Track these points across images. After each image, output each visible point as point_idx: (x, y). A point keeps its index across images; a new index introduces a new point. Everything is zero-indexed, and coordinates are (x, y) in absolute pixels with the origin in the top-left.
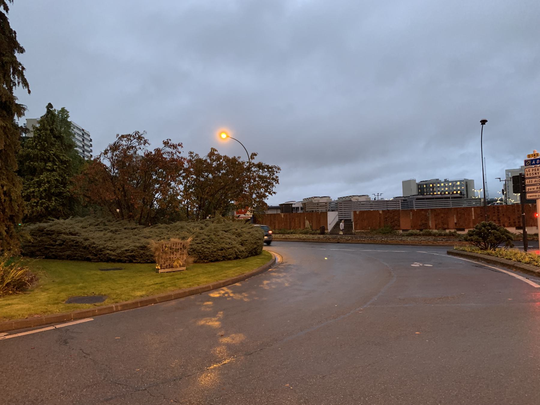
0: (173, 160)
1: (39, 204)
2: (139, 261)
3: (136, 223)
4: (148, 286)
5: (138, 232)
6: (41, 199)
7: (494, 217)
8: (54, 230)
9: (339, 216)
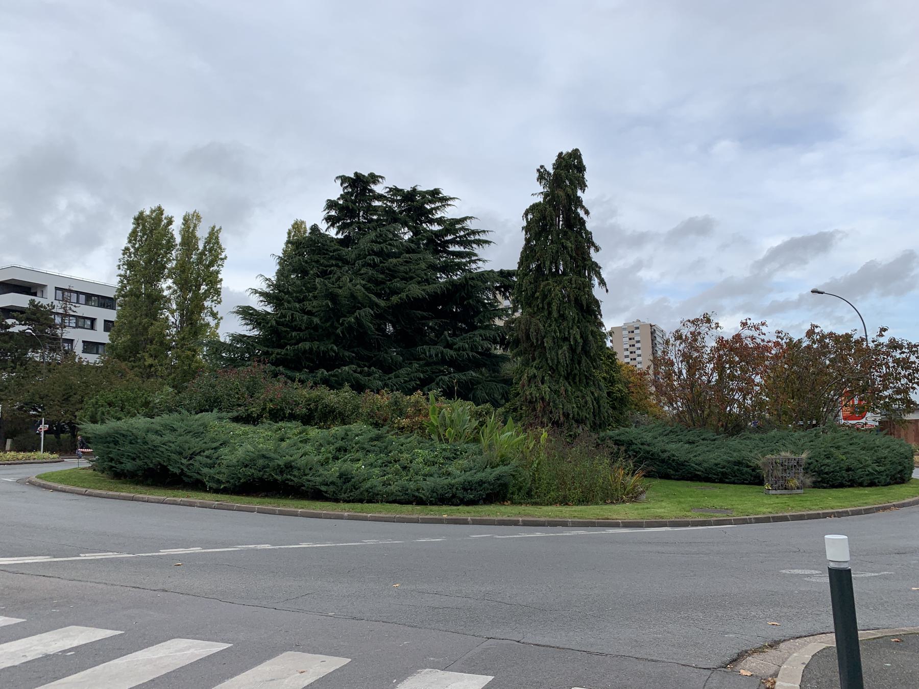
0: (758, 347)
8: (623, 441)
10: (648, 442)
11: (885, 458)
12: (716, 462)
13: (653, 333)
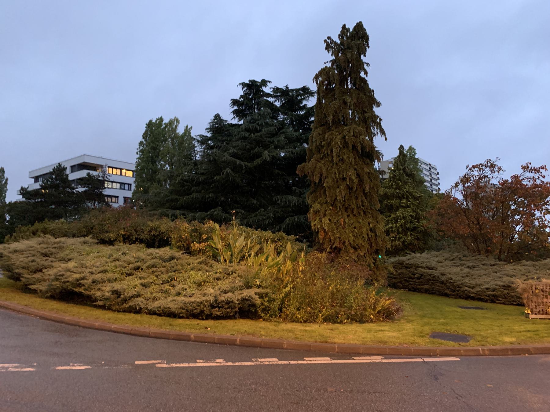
1: (397, 239)
2: (502, 302)
3: (495, 259)
4: (517, 332)
5: (498, 268)
6: (398, 233)
8: (412, 264)
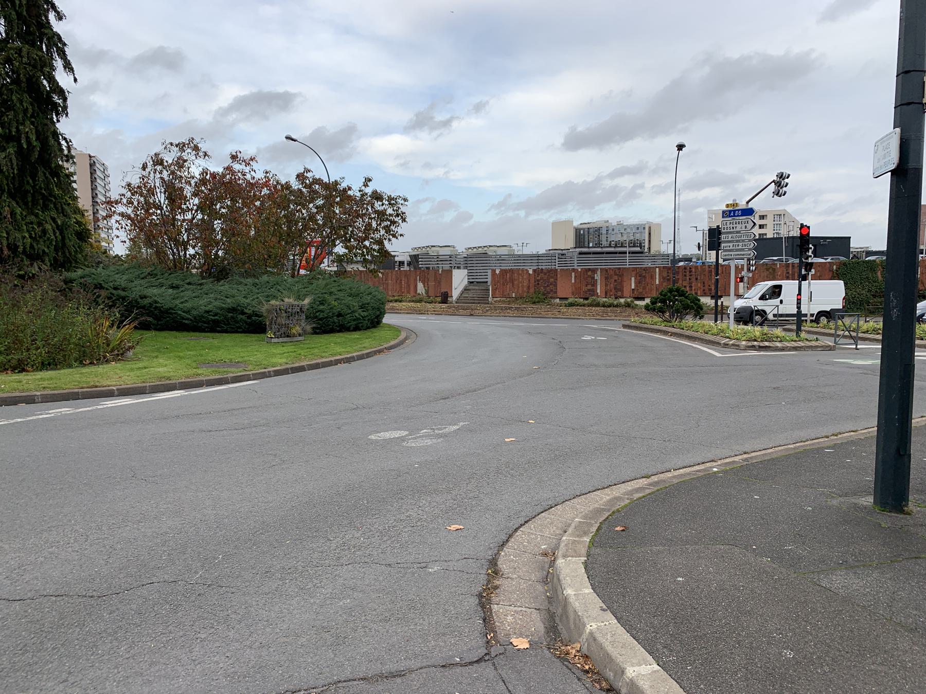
7: (684, 282)
9: (468, 276)
10: (123, 286)
11: (368, 304)
12: (207, 309)
13: (92, 165)
